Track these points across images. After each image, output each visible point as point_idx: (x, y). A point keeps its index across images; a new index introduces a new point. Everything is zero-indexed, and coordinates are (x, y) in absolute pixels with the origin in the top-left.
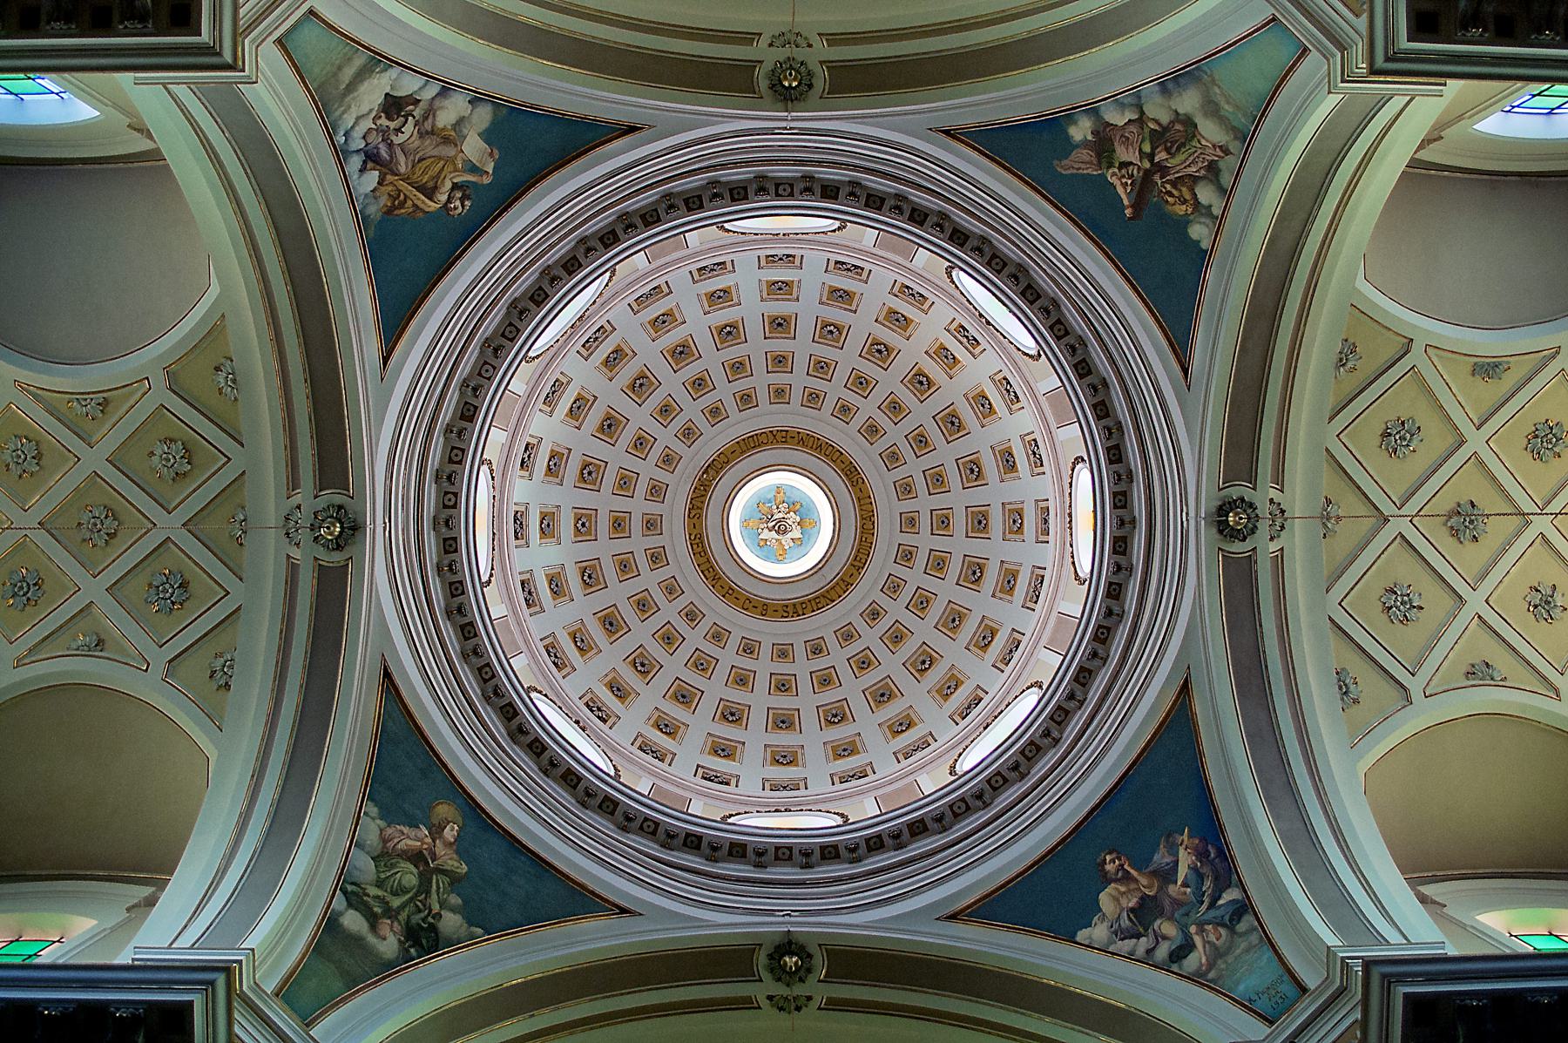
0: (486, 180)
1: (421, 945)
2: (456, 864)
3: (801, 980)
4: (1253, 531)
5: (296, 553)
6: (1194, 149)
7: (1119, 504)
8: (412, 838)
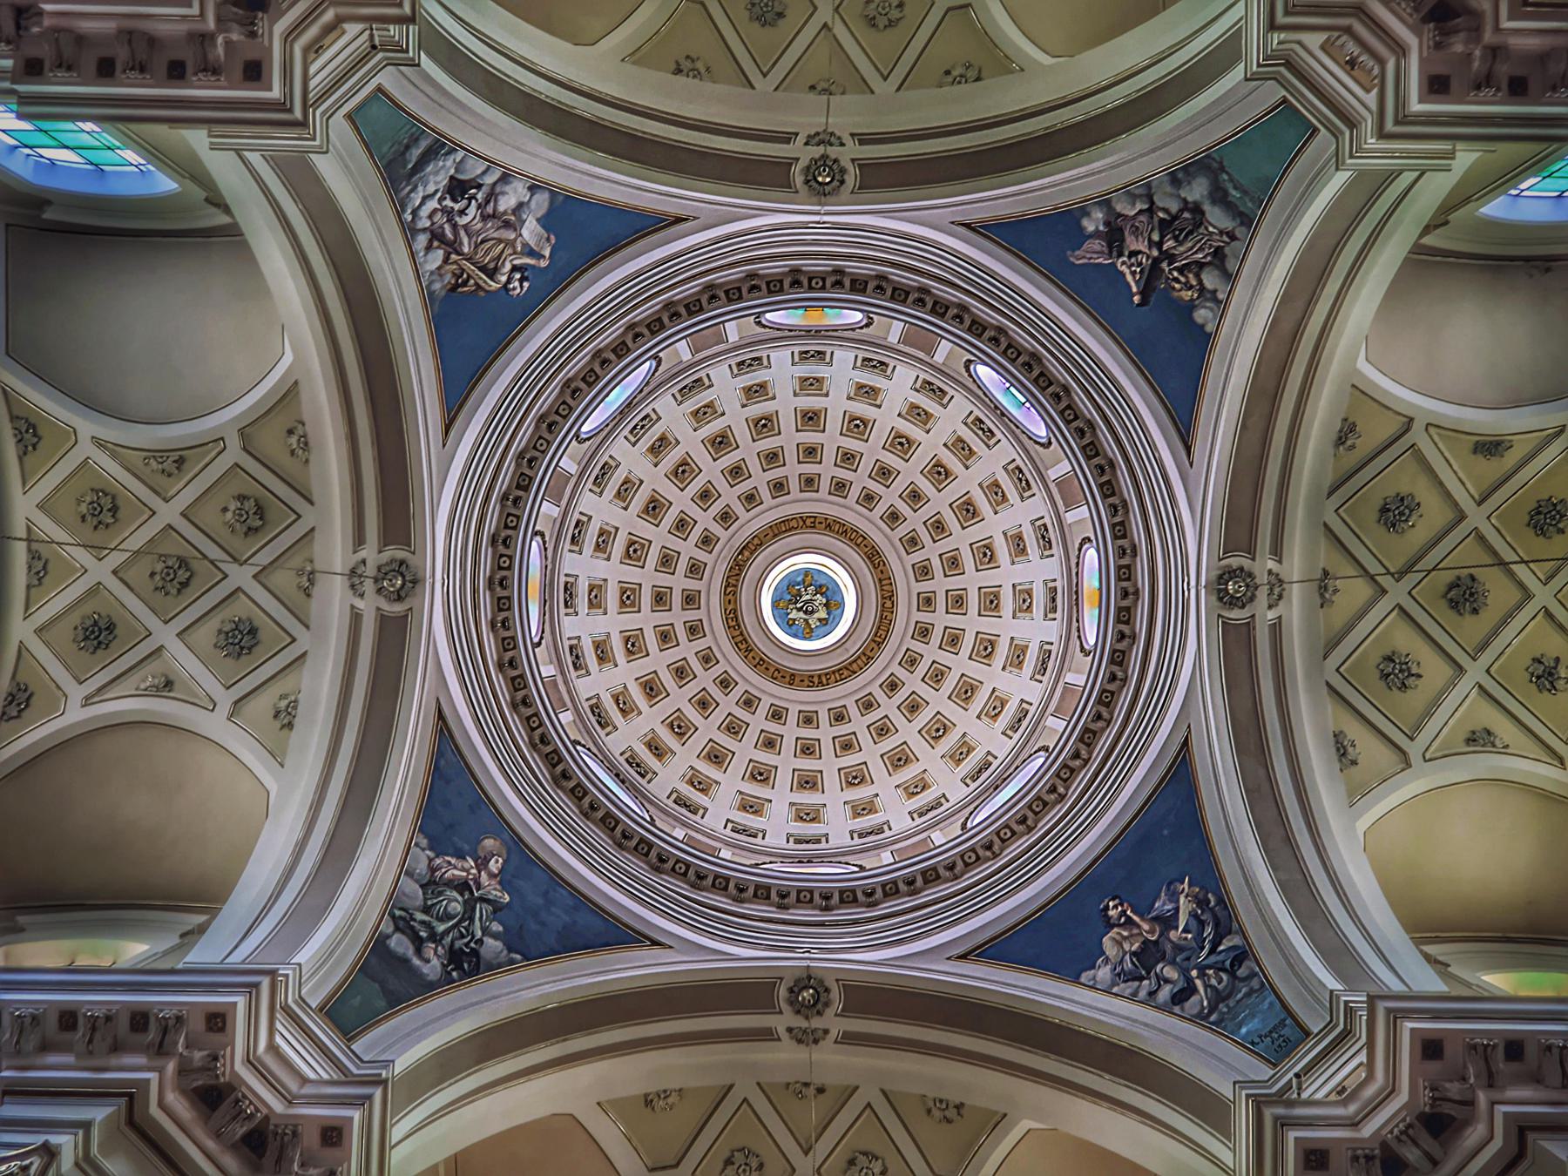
0: (543, 264)
1: (464, 970)
2: (499, 894)
3: (819, 1013)
4: (1252, 599)
5: (360, 604)
6: (1201, 236)
7: (1123, 577)
8: (457, 869)
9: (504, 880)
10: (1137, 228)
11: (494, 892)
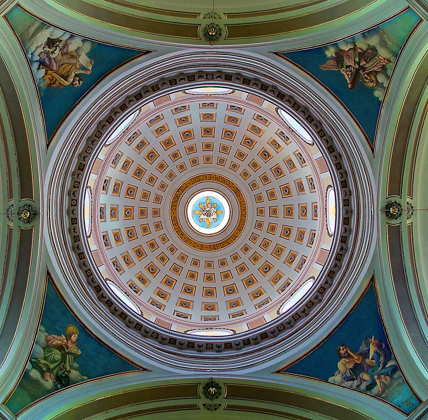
0: (89, 73)
1: (62, 383)
2: (76, 350)
3: (217, 398)
4: (400, 215)
6: (376, 60)
9: (78, 343)
10: (349, 56)
11: (74, 350)
